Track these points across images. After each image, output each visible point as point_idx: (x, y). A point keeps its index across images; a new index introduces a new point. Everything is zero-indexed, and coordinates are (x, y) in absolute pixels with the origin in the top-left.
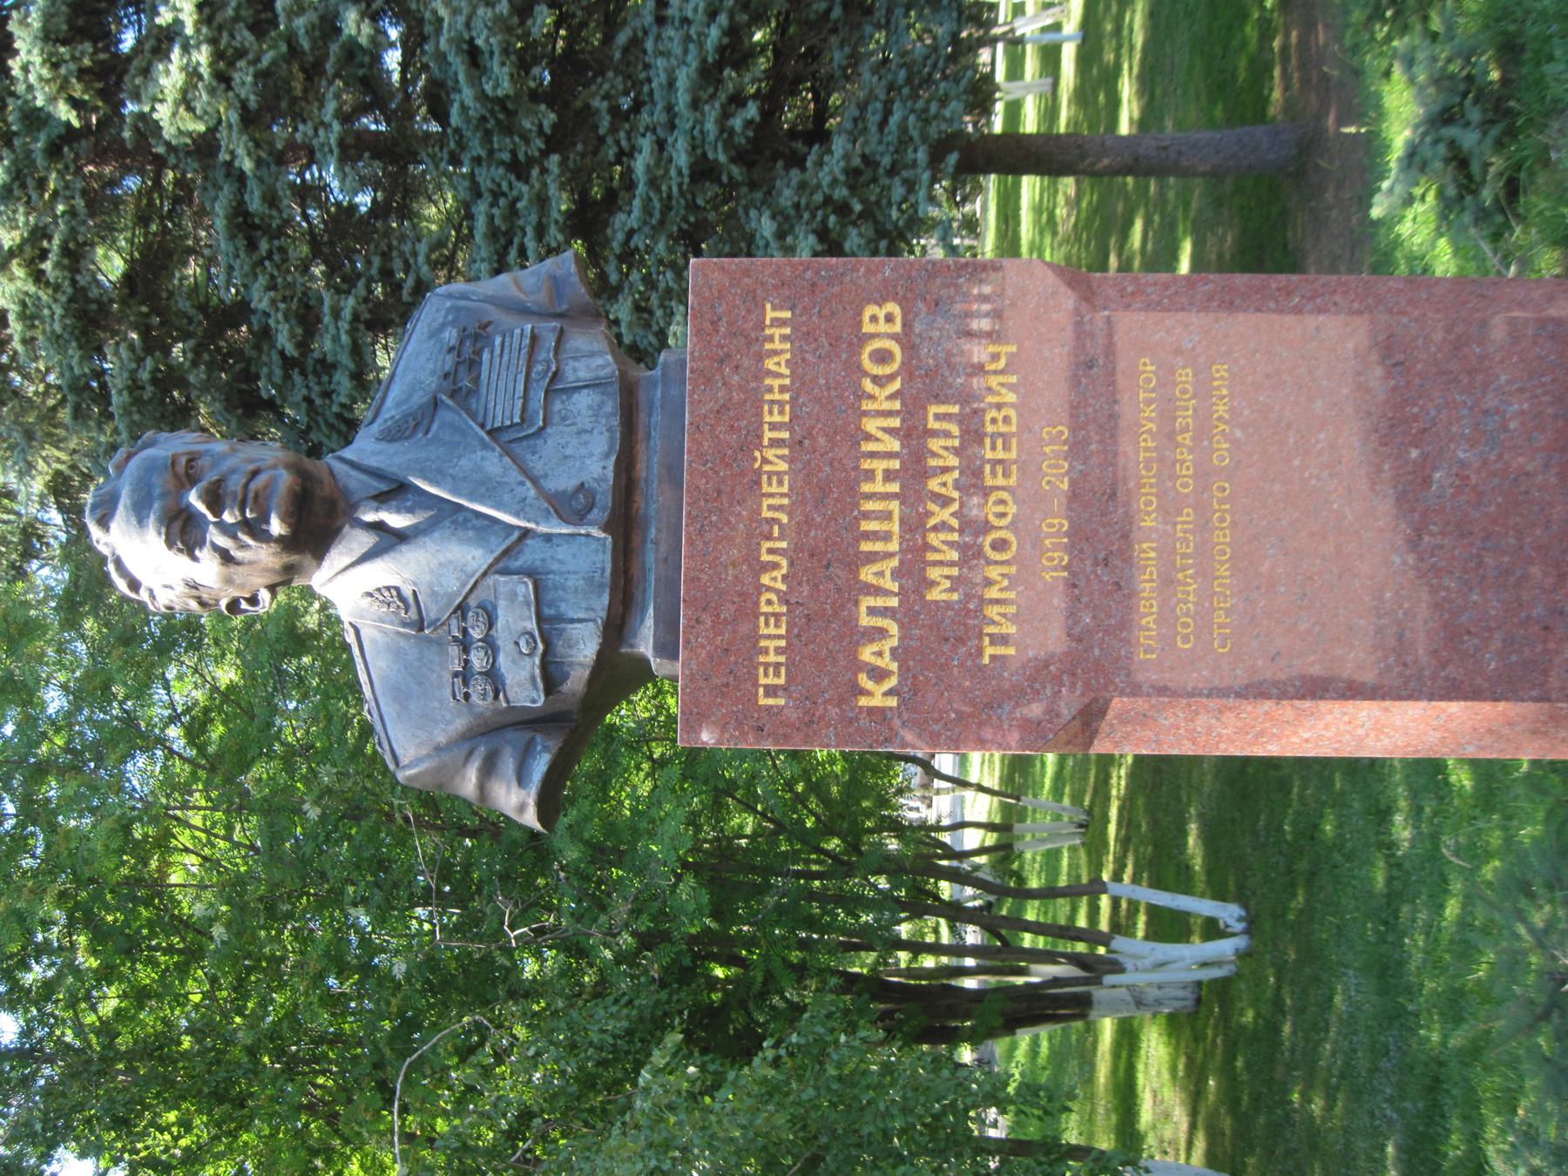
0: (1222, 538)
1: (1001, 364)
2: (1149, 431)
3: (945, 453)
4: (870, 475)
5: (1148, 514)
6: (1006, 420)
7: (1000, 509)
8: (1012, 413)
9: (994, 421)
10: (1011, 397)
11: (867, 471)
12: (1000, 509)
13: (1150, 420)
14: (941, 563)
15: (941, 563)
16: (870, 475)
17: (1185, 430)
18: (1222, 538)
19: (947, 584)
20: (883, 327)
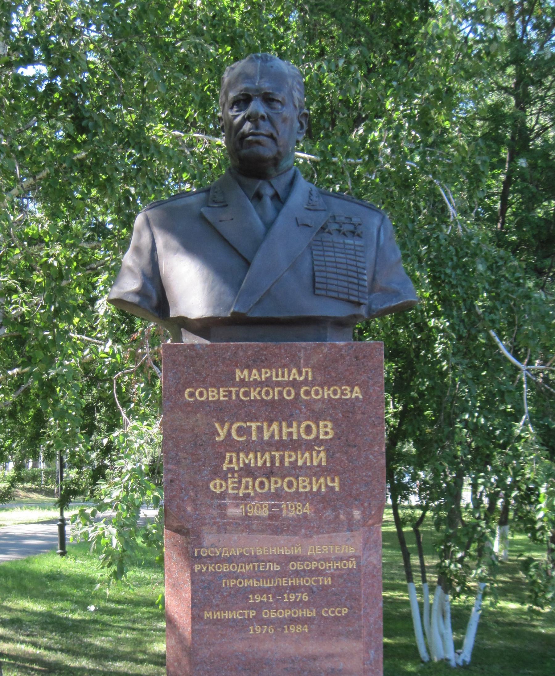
0: (22, 638)
1: (224, 484)
2: (202, 569)
3: (319, 458)
4: (290, 426)
5: (214, 568)
6: (305, 487)
7: (218, 487)
8: (308, 489)
9: (304, 481)
10: (315, 489)
11: (292, 424)
12: (218, 487)
13: (207, 569)
14: (256, 458)
15: (256, 458)
16: (290, 426)
17: (317, 581)
18: (22, 638)
19: (247, 462)
20: (322, 431)
